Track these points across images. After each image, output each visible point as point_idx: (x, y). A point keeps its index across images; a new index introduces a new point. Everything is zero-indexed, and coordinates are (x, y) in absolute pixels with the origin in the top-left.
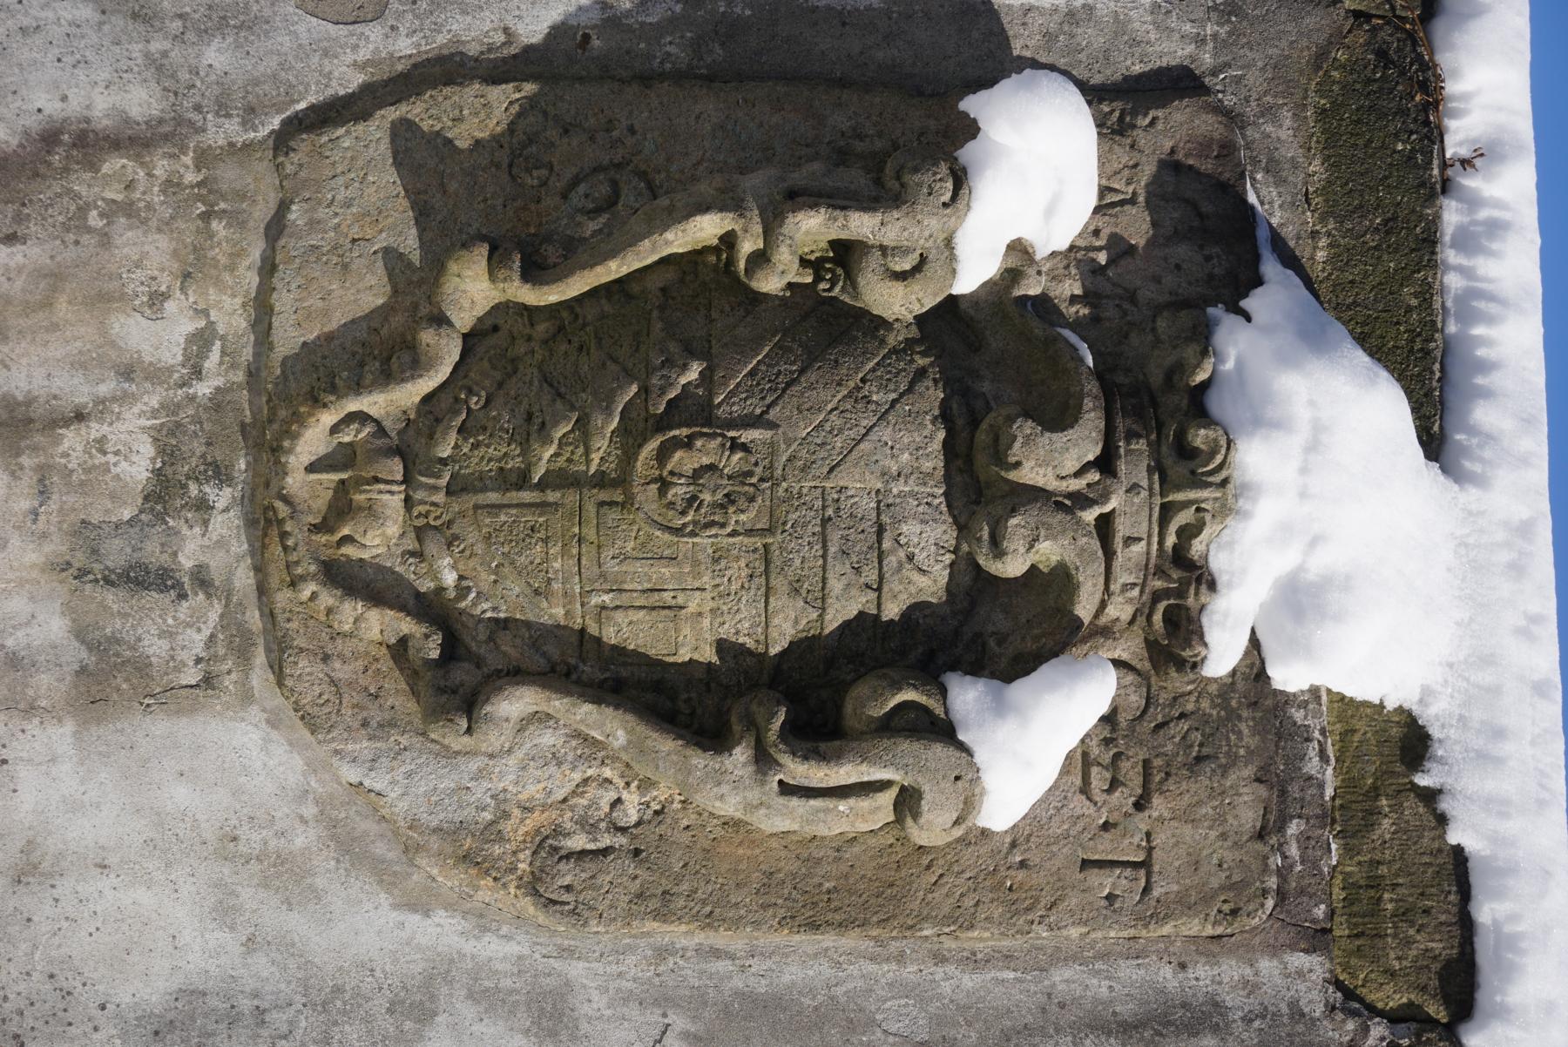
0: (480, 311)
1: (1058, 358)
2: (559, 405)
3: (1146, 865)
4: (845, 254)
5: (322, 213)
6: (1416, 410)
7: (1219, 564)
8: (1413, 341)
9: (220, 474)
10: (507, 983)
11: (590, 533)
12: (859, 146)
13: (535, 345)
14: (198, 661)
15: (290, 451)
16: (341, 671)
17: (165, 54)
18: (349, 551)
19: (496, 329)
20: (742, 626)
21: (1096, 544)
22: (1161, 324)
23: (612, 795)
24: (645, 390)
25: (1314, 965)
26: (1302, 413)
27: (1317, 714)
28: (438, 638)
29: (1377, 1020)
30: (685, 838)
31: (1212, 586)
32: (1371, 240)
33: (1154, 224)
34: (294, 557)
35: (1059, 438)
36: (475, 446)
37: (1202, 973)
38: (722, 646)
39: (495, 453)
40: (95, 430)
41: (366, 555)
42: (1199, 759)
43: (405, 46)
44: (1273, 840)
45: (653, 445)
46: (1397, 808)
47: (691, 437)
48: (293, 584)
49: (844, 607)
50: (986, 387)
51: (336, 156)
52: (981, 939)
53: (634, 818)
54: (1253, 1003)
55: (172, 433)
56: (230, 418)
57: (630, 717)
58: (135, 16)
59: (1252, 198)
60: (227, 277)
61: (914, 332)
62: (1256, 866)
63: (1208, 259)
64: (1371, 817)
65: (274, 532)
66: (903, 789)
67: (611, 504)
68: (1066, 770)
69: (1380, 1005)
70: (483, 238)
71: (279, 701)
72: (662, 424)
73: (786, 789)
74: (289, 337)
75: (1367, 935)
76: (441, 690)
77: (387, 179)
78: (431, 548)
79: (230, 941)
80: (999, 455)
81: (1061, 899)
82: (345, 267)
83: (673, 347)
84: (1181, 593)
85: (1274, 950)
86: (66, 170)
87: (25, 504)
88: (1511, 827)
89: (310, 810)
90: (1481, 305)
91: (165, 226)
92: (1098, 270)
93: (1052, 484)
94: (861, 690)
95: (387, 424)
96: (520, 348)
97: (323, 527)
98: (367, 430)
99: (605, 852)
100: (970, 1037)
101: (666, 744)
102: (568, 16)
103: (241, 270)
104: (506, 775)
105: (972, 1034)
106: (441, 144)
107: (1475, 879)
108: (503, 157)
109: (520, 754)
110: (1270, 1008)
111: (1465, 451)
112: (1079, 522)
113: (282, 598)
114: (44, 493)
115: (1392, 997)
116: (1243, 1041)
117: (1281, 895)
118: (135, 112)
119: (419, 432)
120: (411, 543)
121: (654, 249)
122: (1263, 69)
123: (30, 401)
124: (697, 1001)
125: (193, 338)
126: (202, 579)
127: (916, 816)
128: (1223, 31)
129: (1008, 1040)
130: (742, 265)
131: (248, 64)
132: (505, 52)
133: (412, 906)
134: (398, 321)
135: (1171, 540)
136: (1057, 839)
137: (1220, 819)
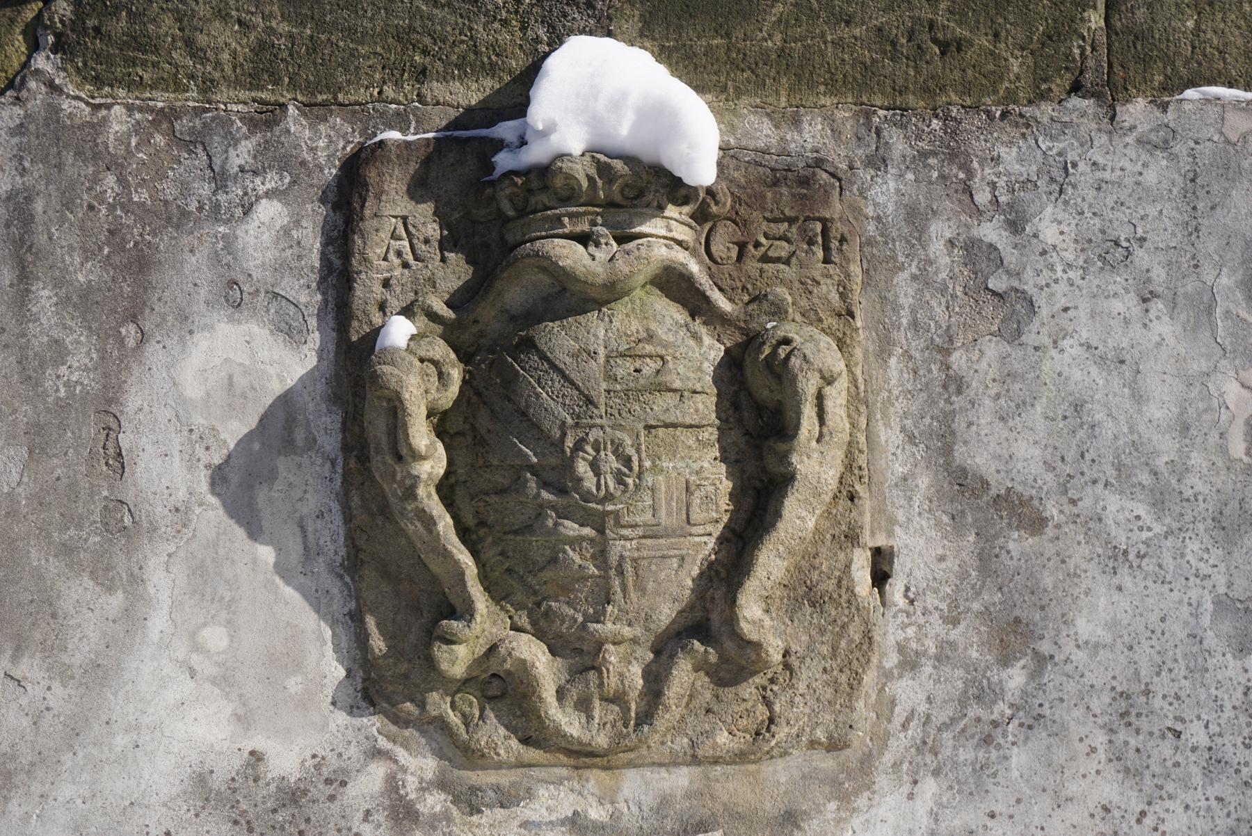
29: (32, 61)
69: (23, 58)
100: (26, 410)
105: (24, 408)
110: (15, 152)
116: (40, 177)
129: (30, 378)
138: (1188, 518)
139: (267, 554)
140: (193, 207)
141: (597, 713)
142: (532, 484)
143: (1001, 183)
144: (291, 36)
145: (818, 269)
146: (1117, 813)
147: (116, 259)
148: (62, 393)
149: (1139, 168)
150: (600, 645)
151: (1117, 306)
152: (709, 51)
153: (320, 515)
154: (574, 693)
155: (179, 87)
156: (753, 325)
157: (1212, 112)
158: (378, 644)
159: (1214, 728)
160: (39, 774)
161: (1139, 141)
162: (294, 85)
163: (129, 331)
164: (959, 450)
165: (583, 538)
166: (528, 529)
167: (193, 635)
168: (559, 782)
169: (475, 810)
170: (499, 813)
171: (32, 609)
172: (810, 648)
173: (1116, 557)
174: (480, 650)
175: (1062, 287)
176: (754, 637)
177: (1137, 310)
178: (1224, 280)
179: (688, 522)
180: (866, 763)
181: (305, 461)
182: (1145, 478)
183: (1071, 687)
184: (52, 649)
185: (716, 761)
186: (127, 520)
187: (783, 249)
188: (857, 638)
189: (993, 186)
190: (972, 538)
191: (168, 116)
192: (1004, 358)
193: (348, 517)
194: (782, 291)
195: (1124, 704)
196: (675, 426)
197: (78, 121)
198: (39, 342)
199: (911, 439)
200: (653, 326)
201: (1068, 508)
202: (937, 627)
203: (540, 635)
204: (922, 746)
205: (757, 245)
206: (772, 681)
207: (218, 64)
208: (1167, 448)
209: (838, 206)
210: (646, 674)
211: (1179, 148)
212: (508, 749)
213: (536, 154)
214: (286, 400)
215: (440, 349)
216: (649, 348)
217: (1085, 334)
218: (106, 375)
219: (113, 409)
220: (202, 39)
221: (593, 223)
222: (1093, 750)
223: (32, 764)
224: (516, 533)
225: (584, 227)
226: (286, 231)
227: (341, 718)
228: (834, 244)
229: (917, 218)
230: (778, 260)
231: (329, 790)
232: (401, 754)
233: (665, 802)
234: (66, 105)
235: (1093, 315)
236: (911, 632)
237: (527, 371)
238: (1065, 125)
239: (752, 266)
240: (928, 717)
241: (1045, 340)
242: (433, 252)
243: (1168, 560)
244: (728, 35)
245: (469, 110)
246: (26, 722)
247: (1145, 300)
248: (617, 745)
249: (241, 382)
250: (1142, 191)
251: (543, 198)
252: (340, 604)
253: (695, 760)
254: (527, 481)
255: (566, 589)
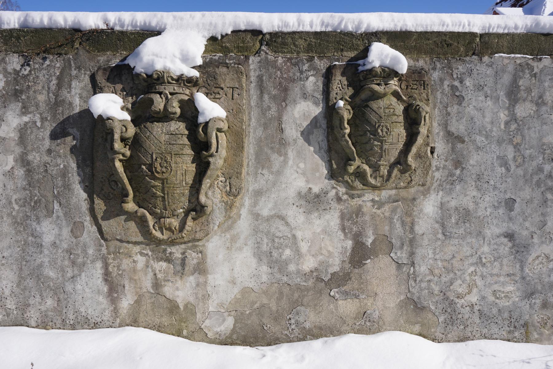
0: (135, 205)
1: (143, 101)
2: (150, 191)
3: (233, 88)
4: (123, 140)
5: (118, 233)
6: (153, 36)
7: (178, 74)
8: (140, 37)
9: (165, 251)
10: (253, 201)
11: (172, 185)
12: (105, 137)
13: (140, 195)
14: (197, 254)
15: (160, 238)
16: (198, 229)
17: (90, 260)
18: (177, 228)
19: (138, 202)
20: (189, 159)
21: (175, 96)
22: (136, 82)
23: (220, 182)
24: (147, 176)
25: (251, 59)
26: (151, 57)
27: (207, 56)
28: (192, 212)
30: (227, 170)
31: (182, 75)
32: (122, 43)
33: (118, 83)
34: (178, 237)
35: (155, 102)
36: (158, 206)
37: (253, 79)
38: (193, 163)
39: (159, 202)
40: (157, 272)
41: (178, 225)
42: (214, 78)
43: (88, 218)
44: (229, 65)
45: (156, 174)
46: (225, 43)
47: (155, 168)
48: (183, 238)
49: (186, 141)
50: (148, 115)
51: (108, 230)
52: (246, 118)
53: (224, 179)
54: (258, 70)
55: (158, 259)
56: (155, 249)
57: (204, 179)
58: (84, 266)
59: (114, 65)
60: (130, 249)
61: (138, 127)
62: (233, 69)
63: (125, 74)
64: (226, 47)
65: (174, 241)
66: (217, 131)
67: (167, 182)
68: (216, 102)
70: (121, 204)
71: (204, 240)
72: (152, 173)
73: (217, 152)
74: (140, 239)
75: (247, 49)
76: (201, 212)
77: (112, 221)
78: (176, 213)
79: (245, 248)
80: (158, 113)
81: (238, 103)
82: (128, 229)
83: (139, 171)
84: (184, 80)
85: (249, 66)
86: (112, 277)
87: (170, 283)
88: (227, 22)
89: (223, 235)
90: (134, 23)
91: (121, 260)
92: (127, 94)
93: (164, 103)
94: (200, 138)
95: (155, 221)
96: (141, 198)
97: (173, 232)
98: (156, 225)
99: (230, 184)
101: (209, 172)
102: (82, 189)
103: (129, 247)
104: (217, 201)
106: (105, 212)
107: (237, 29)
108: (107, 201)
109: (213, 198)
111: (160, 28)
112: (170, 99)
113: (186, 239)
114: (169, 280)
115: (258, 45)
117: (239, 64)
118: (101, 265)
119: (156, 216)
120: (176, 217)
121: (122, 174)
122: (90, 62)
123: (152, 283)
124: (256, 168)
125: (141, 255)
126: (183, 253)
127: (222, 129)
128: (83, 69)
130: (125, 158)
131: (92, 246)
132: (89, 200)
133: (240, 217)
134: (137, 220)
135: (174, 82)
136: (228, 104)
137: (225, 75)
138: (492, 140)
139: (312, 149)
140: (296, 78)
141: (378, 179)
142: (369, 134)
143: (459, 73)
144: (315, 42)
145: (422, 91)
146: (476, 198)
147: (281, 89)
148: (270, 117)
149: (486, 70)
150: (379, 166)
151: (480, 98)
152: (400, 45)
153: (322, 141)
154: (374, 175)
155: (292, 53)
156: (410, 102)
157: (501, 59)
158: (335, 166)
159: (495, 181)
160: (268, 192)
161: (486, 65)
162: (316, 53)
163: (284, 104)
164: (449, 127)
165: (378, 145)
166: (367, 143)
167: (297, 165)
168: (370, 193)
169: (353, 198)
170: (358, 199)
171: (265, 160)
172: (419, 166)
173: (478, 148)
174: (356, 167)
175: (470, 94)
176: (410, 164)
177: (484, 99)
178: (502, 93)
179: (398, 141)
180: (429, 189)
181: (319, 130)
182: (484, 133)
183: (468, 173)
184: (270, 168)
185: (400, 188)
186: (284, 142)
187: (415, 87)
188: (428, 164)
189: (457, 74)
190: (450, 145)
191: (290, 59)
192: (458, 109)
193: (328, 141)
194: (415, 95)
195: (478, 177)
196: (397, 122)
197: (272, 60)
198: (265, 106)
199: (439, 125)
200: (391, 102)
201: (469, 139)
202: (443, 162)
203: (367, 164)
204: (440, 185)
205: (410, 86)
206: (412, 173)
207: (300, 48)
208: (489, 127)
209: (426, 78)
210: (388, 171)
211: (494, 66)
212: (360, 187)
213: (369, 67)
214: (315, 117)
215: (349, 107)
216: (392, 107)
217: (474, 104)
218: (279, 113)
219: (281, 120)
220: (297, 43)
221: (380, 81)
222: (472, 185)
223: (266, 191)
224: (364, 144)
225: (378, 82)
226: (315, 83)
227: (327, 181)
228: (426, 86)
229: (442, 80)
230: (414, 89)
231: (325, 195)
232: (338, 188)
233: (390, 196)
234: (269, 57)
235: (476, 100)
236: (438, 163)
237: (367, 111)
238: (472, 61)
239: (409, 90)
240: (441, 179)
241: (466, 105)
242: (346, 87)
243: (488, 149)
244: (404, 42)
245: (352, 58)
246: (265, 182)
247: (486, 97)
248: (382, 185)
249: (306, 114)
250: (487, 76)
251: (370, 76)
252: (326, 159)
253: (396, 188)
254: (367, 134)
255: (373, 155)
